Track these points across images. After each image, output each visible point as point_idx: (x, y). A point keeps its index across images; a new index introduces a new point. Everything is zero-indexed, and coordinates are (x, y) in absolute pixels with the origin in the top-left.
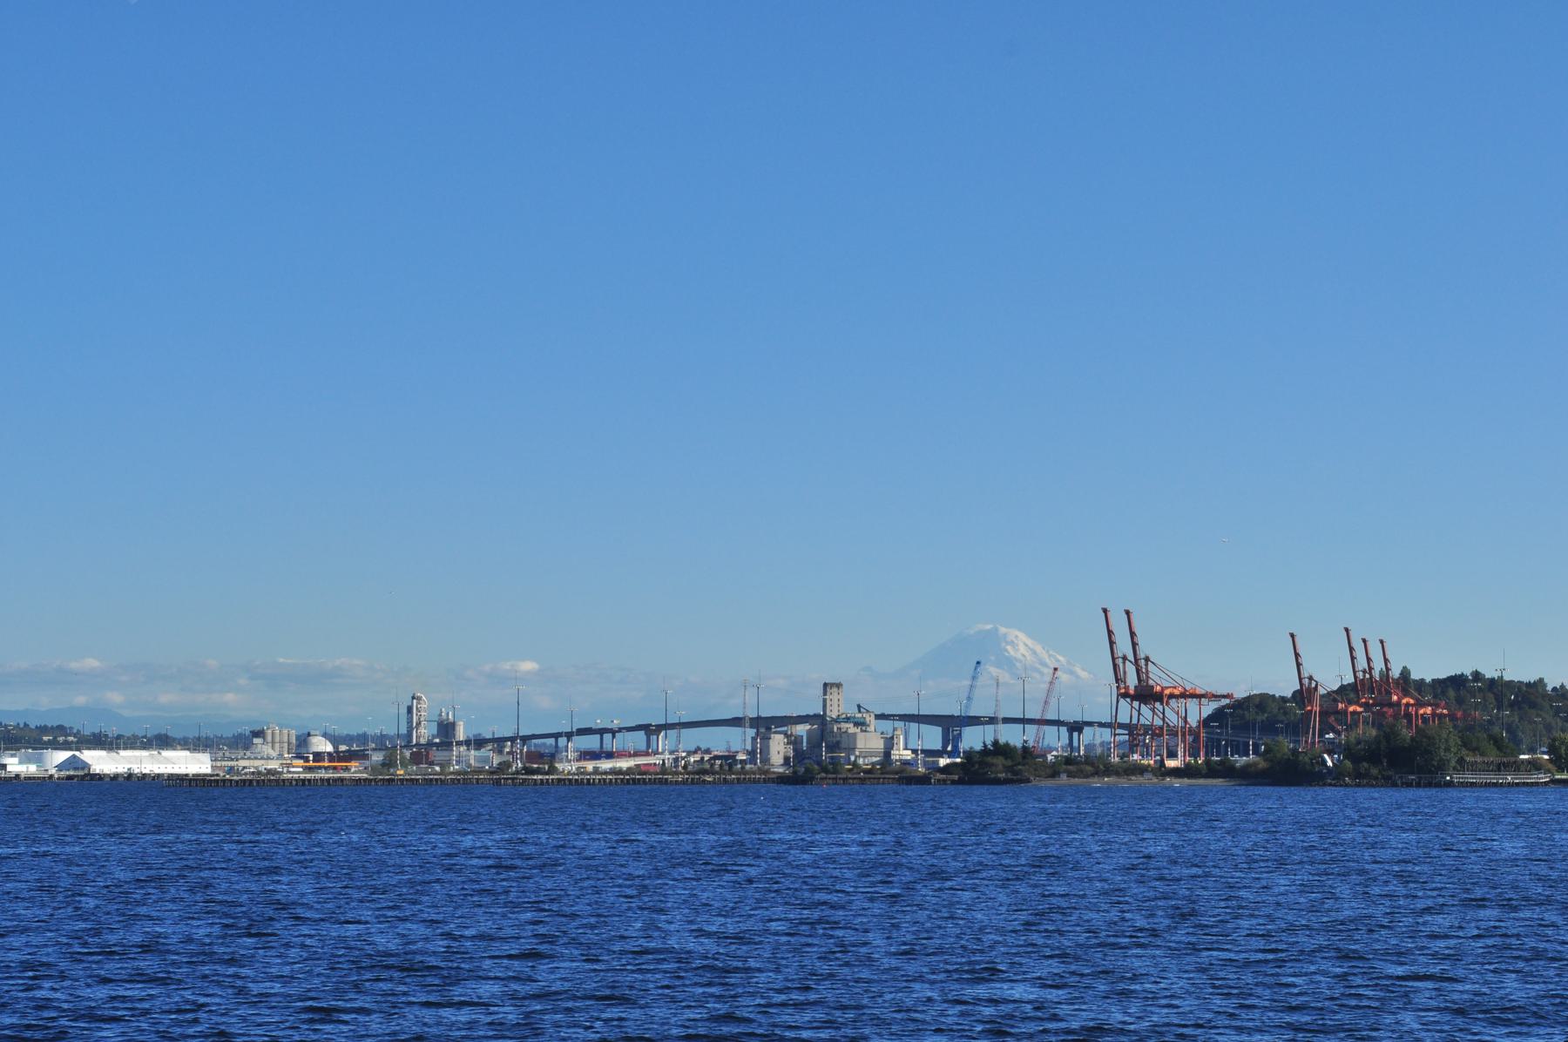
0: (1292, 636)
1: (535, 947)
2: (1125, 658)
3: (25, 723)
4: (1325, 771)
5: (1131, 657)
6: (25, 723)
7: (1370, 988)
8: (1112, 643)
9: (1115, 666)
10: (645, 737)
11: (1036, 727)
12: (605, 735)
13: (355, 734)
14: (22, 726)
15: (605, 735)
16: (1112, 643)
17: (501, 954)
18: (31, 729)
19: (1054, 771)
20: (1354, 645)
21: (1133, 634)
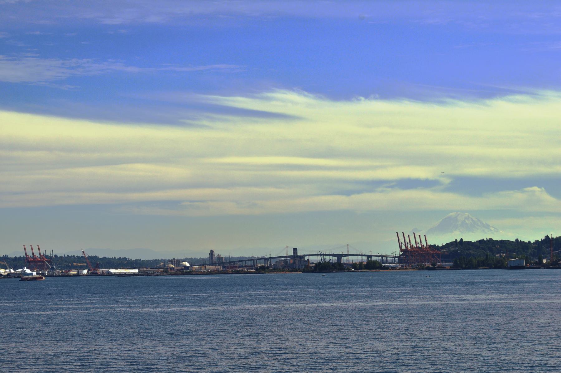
0: (397, 233)
1: (125, 366)
2: (407, 243)
3: (114, 257)
4: (66, 270)
5: (409, 243)
6: (114, 257)
7: (117, 372)
8: (415, 240)
9: (399, 245)
10: (264, 261)
11: (317, 256)
12: (243, 262)
13: (13, 257)
14: (113, 258)
15: (243, 262)
16: (415, 240)
17: (503, 280)
18: (116, 259)
19: (100, 275)
20: (405, 237)
21: (426, 240)
